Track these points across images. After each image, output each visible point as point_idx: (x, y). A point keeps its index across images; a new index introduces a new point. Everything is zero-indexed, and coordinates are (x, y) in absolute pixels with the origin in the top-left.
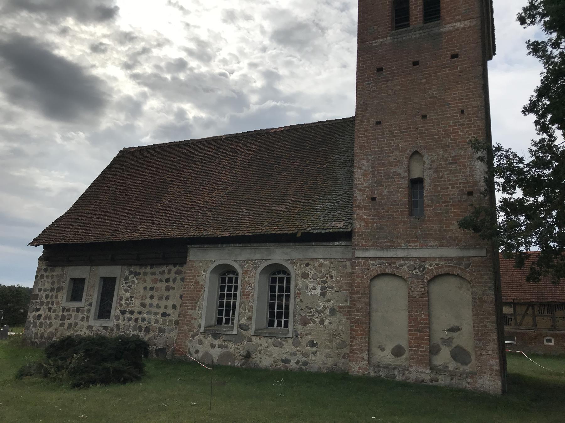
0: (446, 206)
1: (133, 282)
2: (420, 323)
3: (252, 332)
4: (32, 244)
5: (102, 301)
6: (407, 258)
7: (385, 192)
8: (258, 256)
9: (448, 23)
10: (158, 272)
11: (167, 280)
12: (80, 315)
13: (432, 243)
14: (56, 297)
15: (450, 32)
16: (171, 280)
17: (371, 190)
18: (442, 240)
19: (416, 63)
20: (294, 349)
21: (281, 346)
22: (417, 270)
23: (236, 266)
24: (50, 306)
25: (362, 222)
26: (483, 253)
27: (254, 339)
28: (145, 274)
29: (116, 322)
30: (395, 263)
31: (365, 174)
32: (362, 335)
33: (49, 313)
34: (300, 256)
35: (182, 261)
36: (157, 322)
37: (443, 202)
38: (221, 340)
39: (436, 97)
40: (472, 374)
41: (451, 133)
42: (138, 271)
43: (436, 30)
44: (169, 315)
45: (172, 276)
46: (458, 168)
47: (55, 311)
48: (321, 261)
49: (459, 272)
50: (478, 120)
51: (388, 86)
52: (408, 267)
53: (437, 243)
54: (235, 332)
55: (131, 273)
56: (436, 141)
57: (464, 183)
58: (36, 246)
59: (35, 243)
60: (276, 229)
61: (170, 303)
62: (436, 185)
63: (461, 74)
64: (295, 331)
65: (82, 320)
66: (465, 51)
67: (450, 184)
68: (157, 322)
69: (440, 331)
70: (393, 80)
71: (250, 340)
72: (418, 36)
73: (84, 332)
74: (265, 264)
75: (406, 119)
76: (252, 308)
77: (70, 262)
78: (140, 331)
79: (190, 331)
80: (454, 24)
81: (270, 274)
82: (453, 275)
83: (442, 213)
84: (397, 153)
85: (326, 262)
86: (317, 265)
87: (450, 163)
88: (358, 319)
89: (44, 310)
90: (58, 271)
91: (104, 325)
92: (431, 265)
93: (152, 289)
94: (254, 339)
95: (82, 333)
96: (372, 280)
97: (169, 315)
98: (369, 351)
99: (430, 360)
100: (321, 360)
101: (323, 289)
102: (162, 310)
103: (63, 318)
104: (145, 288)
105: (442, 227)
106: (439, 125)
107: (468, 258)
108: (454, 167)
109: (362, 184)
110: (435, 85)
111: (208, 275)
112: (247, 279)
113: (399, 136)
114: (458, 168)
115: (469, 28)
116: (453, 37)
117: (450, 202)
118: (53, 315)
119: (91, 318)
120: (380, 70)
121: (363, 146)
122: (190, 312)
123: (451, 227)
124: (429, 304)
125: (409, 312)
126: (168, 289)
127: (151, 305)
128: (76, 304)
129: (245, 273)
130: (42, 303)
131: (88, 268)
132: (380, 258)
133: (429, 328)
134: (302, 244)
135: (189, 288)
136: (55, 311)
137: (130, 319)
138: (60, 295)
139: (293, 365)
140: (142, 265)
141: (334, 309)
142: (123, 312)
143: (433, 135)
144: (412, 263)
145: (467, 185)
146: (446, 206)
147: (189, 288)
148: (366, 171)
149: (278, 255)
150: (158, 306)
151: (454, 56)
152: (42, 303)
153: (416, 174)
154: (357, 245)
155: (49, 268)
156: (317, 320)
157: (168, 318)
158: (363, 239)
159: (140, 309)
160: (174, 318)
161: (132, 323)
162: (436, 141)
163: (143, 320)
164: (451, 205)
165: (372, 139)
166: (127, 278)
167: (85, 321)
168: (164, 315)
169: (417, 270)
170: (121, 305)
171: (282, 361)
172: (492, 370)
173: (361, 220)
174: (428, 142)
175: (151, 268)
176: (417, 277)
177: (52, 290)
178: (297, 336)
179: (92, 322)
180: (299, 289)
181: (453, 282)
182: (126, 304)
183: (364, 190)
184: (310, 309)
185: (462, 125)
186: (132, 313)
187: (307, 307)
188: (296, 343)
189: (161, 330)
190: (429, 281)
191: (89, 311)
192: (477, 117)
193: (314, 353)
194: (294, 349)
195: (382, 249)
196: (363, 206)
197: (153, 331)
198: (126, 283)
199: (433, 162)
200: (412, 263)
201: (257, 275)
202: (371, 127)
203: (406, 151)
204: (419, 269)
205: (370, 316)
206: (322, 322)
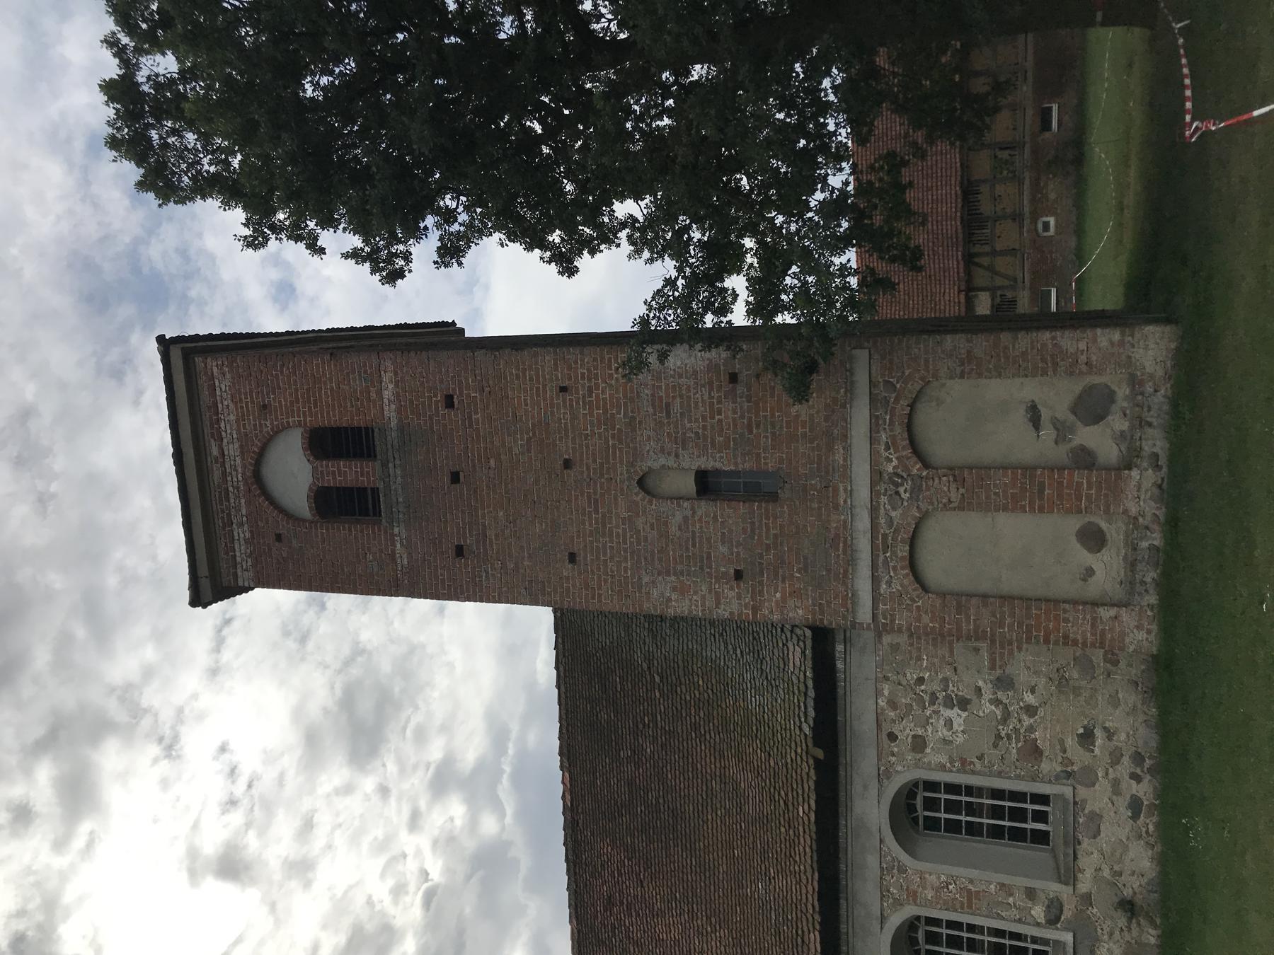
0: (758, 426)
3: (1064, 892)
6: (874, 510)
7: (723, 549)
8: (872, 861)
18: (833, 435)
19: (455, 478)
20: (1103, 786)
21: (1095, 818)
22: (901, 490)
25: (791, 602)
26: (862, 355)
27: (1083, 887)
30: (885, 536)
31: (682, 590)
32: (1057, 617)
34: (872, 753)
37: (751, 432)
39: (529, 439)
41: (605, 412)
46: (678, 400)
48: (882, 703)
49: (903, 402)
51: (497, 535)
52: (894, 509)
53: (839, 448)
54: (1068, 938)
56: (620, 441)
57: (711, 389)
60: (806, 811)
63: (487, 389)
64: (1057, 779)
69: (1040, 447)
70: (484, 526)
71: (1087, 899)
75: (569, 501)
76: (1003, 885)
81: (917, 832)
82: (910, 416)
83: (773, 434)
84: (639, 522)
85: (886, 693)
87: (668, 413)
94: (1083, 887)
96: (925, 589)
98: (1095, 604)
99: (1108, 469)
100: (1126, 720)
101: (949, 703)
105: (804, 435)
108: (676, 407)
109: (703, 597)
112: (930, 894)
114: (678, 400)
115: (396, 374)
116: (411, 402)
129: (913, 896)
132: (874, 567)
133: (1035, 468)
144: (884, 499)
145: (716, 384)
146: (758, 426)
148: (674, 589)
149: (869, 809)
151: (449, 402)
153: (688, 484)
154: (844, 618)
156: (1027, 721)
158: (829, 603)
162: (620, 441)
164: (757, 415)
171: (1135, 817)
172: (1121, 343)
173: (788, 605)
174: (621, 461)
176: (916, 491)
180: (952, 762)
181: (932, 536)
185: (590, 390)
187: (995, 746)
190: (926, 465)
193: (1110, 734)
194: (1103, 786)
195: (851, 561)
199: (662, 450)
200: (884, 499)
203: (636, 503)
204: (897, 485)
205: (1011, 598)
206: (1030, 710)
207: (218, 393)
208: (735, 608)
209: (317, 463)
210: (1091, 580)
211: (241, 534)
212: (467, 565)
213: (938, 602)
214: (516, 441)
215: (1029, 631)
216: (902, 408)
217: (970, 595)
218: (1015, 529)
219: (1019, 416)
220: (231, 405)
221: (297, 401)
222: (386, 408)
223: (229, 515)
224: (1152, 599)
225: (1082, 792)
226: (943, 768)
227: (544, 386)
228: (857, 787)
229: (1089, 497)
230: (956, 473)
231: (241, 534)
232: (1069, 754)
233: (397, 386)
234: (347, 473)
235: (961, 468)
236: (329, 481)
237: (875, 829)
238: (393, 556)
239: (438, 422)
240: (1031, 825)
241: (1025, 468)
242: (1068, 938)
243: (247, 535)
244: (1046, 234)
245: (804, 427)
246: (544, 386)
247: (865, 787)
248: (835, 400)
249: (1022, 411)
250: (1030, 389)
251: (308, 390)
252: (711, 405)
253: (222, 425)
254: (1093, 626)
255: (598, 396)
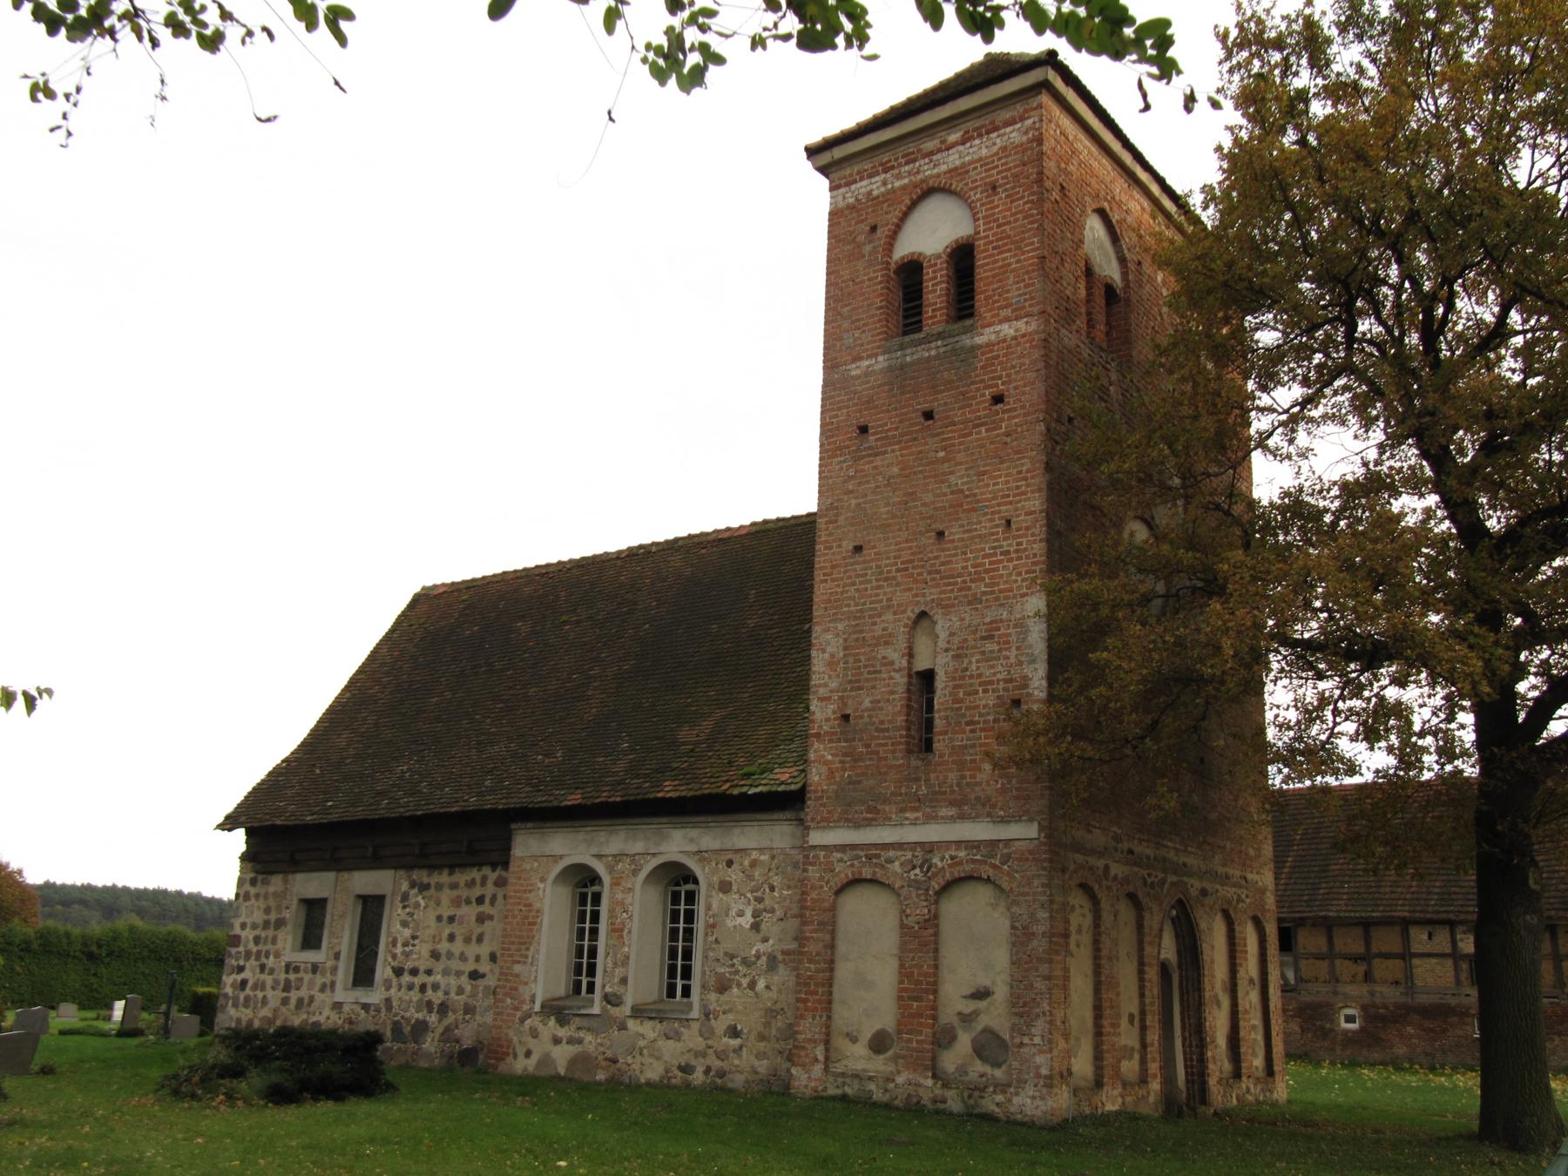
0: (973, 731)
1: (417, 905)
2: (918, 982)
3: (626, 1009)
4: (221, 827)
5: (360, 948)
6: (899, 846)
7: (867, 703)
8: (639, 847)
9: (989, 325)
11: (480, 900)
12: (319, 980)
13: (944, 812)
14: (274, 941)
16: (487, 900)
17: (841, 698)
18: (966, 805)
19: (928, 415)
21: (677, 1036)
22: (917, 871)
23: (600, 868)
24: (264, 960)
25: (824, 769)
27: (631, 1023)
28: (439, 887)
30: (878, 856)
31: (831, 664)
32: (815, 1009)
33: (262, 977)
34: (716, 845)
35: (502, 860)
36: (460, 991)
37: (968, 724)
38: (573, 1027)
39: (962, 491)
40: (1002, 1087)
41: (987, 571)
42: (425, 880)
43: (966, 341)
44: (483, 976)
45: (490, 889)
46: (996, 648)
47: (272, 971)
48: (754, 855)
49: (991, 872)
51: (876, 468)
53: (952, 811)
54: (596, 1010)
55: (413, 886)
56: (960, 590)
57: (1006, 681)
58: (230, 830)
59: (229, 824)
61: (484, 950)
62: (956, 687)
63: (1008, 440)
65: (322, 990)
66: (1016, 388)
67: (980, 684)
68: (460, 991)
69: (953, 997)
70: (885, 452)
72: (933, 353)
73: (325, 1017)
74: (654, 862)
76: (628, 958)
77: (294, 864)
78: (430, 1011)
79: (516, 1009)
80: (998, 328)
81: (668, 885)
82: (979, 879)
83: (965, 747)
84: (889, 616)
85: (762, 858)
86: (746, 863)
87: (983, 638)
88: (810, 977)
90: (276, 883)
91: (364, 1000)
92: (942, 859)
93: (451, 919)
94: (631, 1023)
95: (322, 1019)
97: (483, 976)
98: (827, 1042)
99: (934, 1059)
100: (748, 1064)
101: (756, 915)
102: (470, 966)
104: (439, 918)
105: (963, 777)
107: (1008, 842)
108: (990, 646)
109: (825, 685)
110: (961, 464)
111: (548, 890)
112: (619, 896)
113: (894, 578)
114: (996, 648)
115: (1024, 336)
118: (269, 980)
119: (339, 986)
120: (864, 430)
121: (829, 601)
122: (517, 968)
124: (936, 943)
125: (900, 959)
126: (481, 919)
127: (450, 955)
128: (311, 956)
130: (248, 954)
131: (332, 875)
132: (853, 847)
133: (935, 992)
134: (721, 818)
135: (514, 917)
136: (272, 971)
137: (410, 987)
138: (281, 934)
139: (698, 1077)
140: (433, 868)
142: (398, 972)
143: (952, 577)
144: (909, 855)
146: (973, 731)
147: (514, 917)
148: (832, 656)
149: (678, 843)
150: (463, 957)
151: (998, 399)
152: (248, 954)
153: (922, 664)
154: (813, 820)
155: (260, 877)
156: (745, 982)
157: (481, 982)
158: (824, 805)
159: (430, 963)
160: (491, 981)
161: (415, 995)
162: (960, 590)
163: (436, 987)
164: (982, 730)
166: (405, 897)
167: (328, 991)
168: (475, 975)
169: (917, 871)
170: (394, 957)
171: (680, 1068)
172: (1038, 1076)
173: (822, 765)
175: (450, 874)
176: (916, 884)
177: (266, 924)
178: (707, 1015)
179: (340, 995)
180: (714, 916)
181: (983, 893)
182: (404, 953)
183: (828, 699)
184: (732, 957)
186: (414, 972)
187: (726, 954)
189: (469, 1010)
190: (939, 893)
191: (334, 970)
195: (857, 825)
197: (454, 1012)
198: (404, 907)
199: (952, 634)
200: (909, 855)
201: (638, 887)
203: (904, 612)
204: (921, 867)
205: (832, 970)
206: (752, 985)
207: (1008, 129)
208: (818, 716)
209: (944, 257)
210: (847, 1042)
212: (850, 439)
213: (826, 905)
214: (962, 477)
215: (807, 985)
216: (986, 871)
217: (833, 933)
218: (885, 976)
219: (984, 981)
220: (995, 149)
221: (999, 226)
223: (893, 168)
224: (832, 1091)
225: (695, 1026)
226: (709, 908)
228: (693, 833)
229: (910, 1041)
230: (933, 921)
233: (1015, 338)
234: (936, 291)
235: (937, 926)
236: (928, 273)
237: (662, 849)
238: (857, 359)
239: (978, 390)
240: (679, 984)
241: (935, 983)
243: (875, 193)
244: (1342, 1018)
247: (692, 840)
248: (993, 806)
249: (988, 983)
250: (1001, 993)
251: (1008, 237)
252: (991, 683)
254: (810, 1040)
255: (1001, 561)
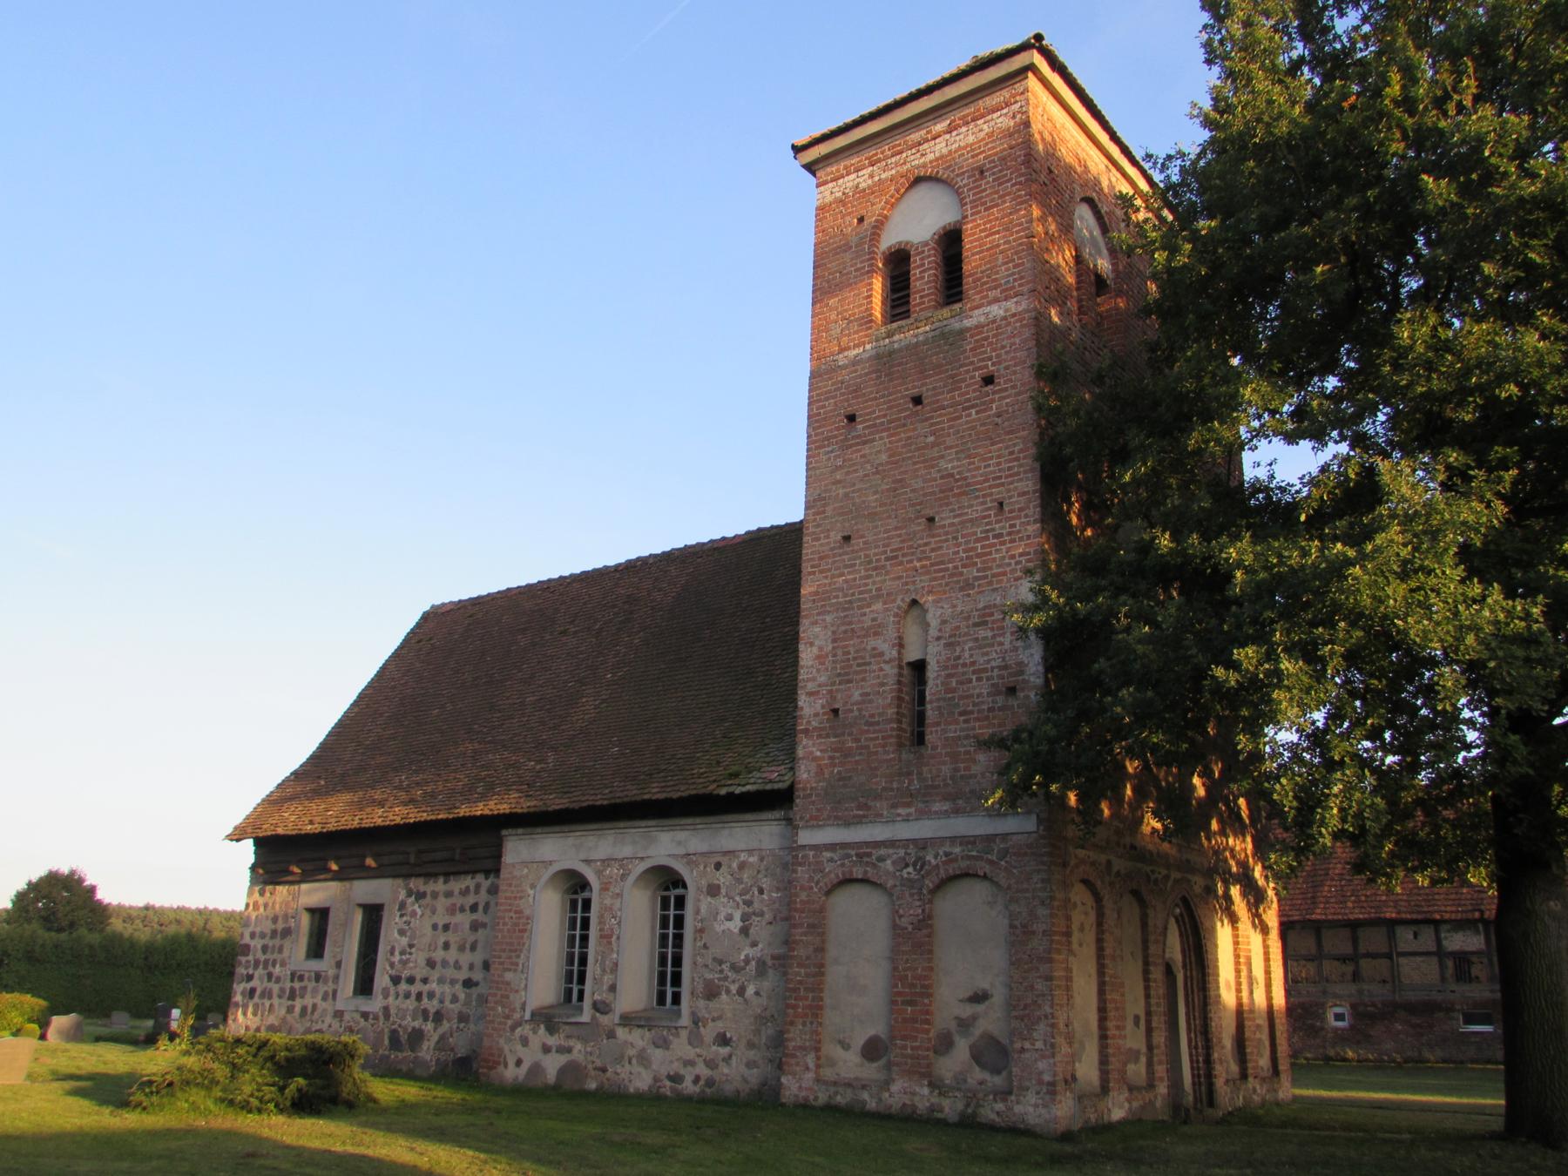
0: (966, 721)
1: (414, 914)
2: (913, 986)
6: (892, 843)
7: (856, 695)
10: (457, 892)
11: (474, 908)
12: (322, 988)
14: (281, 950)
15: (979, 326)
16: (481, 908)
17: (830, 692)
18: (963, 799)
19: (917, 401)
20: (690, 1052)
22: (910, 869)
25: (813, 767)
26: (1030, 824)
29: (385, 1003)
32: (806, 1015)
34: (704, 848)
35: (492, 865)
36: (455, 999)
37: (961, 714)
39: (952, 475)
41: (978, 556)
42: (422, 888)
44: (477, 984)
46: (990, 634)
47: (278, 980)
48: (743, 856)
49: (987, 868)
50: (1028, 523)
52: (894, 863)
53: (946, 806)
54: (585, 1017)
56: (951, 576)
57: (1000, 668)
58: (238, 840)
59: (237, 836)
60: (655, 792)
63: (999, 420)
64: (693, 1014)
66: (1006, 368)
67: (974, 672)
68: (455, 999)
69: (948, 1002)
70: (874, 440)
71: (611, 1035)
75: (896, 528)
78: (426, 1019)
79: (508, 1017)
82: (976, 876)
83: (959, 738)
84: (878, 606)
85: (751, 859)
86: (735, 865)
87: (976, 625)
88: (800, 982)
89: (261, 979)
93: (446, 927)
94: (621, 1033)
96: (828, 893)
97: (477, 984)
101: (745, 918)
103: (292, 997)
104: (435, 927)
105: (956, 770)
106: (956, 538)
107: (1004, 837)
108: (983, 633)
109: (814, 679)
112: (608, 902)
114: (990, 634)
115: (1014, 315)
116: (986, 339)
117: (972, 712)
118: (276, 988)
123: (975, 769)
126: (475, 926)
127: (445, 963)
128: (315, 965)
132: (844, 846)
136: (278, 980)
137: (407, 996)
139: (688, 1087)
140: (430, 876)
141: (764, 963)
142: (396, 980)
143: (942, 563)
145: (1005, 673)
146: (966, 721)
149: (667, 844)
150: (457, 966)
151: (989, 380)
156: (734, 988)
158: (813, 803)
161: (411, 1004)
163: (431, 995)
164: (978, 719)
165: (833, 576)
166: (402, 906)
168: (468, 983)
169: (910, 869)
170: (392, 965)
171: (670, 1078)
173: (811, 760)
174: (935, 579)
175: (445, 882)
176: (909, 883)
182: (400, 961)
184: (721, 962)
185: (1000, 536)
187: (714, 959)
188: (695, 1039)
192: (1026, 516)
194: (690, 1052)
195: (847, 823)
196: (815, 729)
199: (944, 622)
200: (902, 852)
202: (832, 549)
203: (894, 601)
204: (915, 865)
206: (741, 991)
211: (863, 179)
214: (951, 461)
222: (980, 311)
223: (879, 161)
225: (684, 1034)
227: (1002, 485)
228: (681, 835)
229: (904, 1047)
230: (925, 921)
231: (863, 179)
232: (711, 1024)
234: (924, 277)
237: (650, 852)
240: (669, 991)
242: (585, 1017)
245: (966, 769)
246: (1002, 485)
247: (679, 843)
250: (999, 996)
253: (964, 129)
